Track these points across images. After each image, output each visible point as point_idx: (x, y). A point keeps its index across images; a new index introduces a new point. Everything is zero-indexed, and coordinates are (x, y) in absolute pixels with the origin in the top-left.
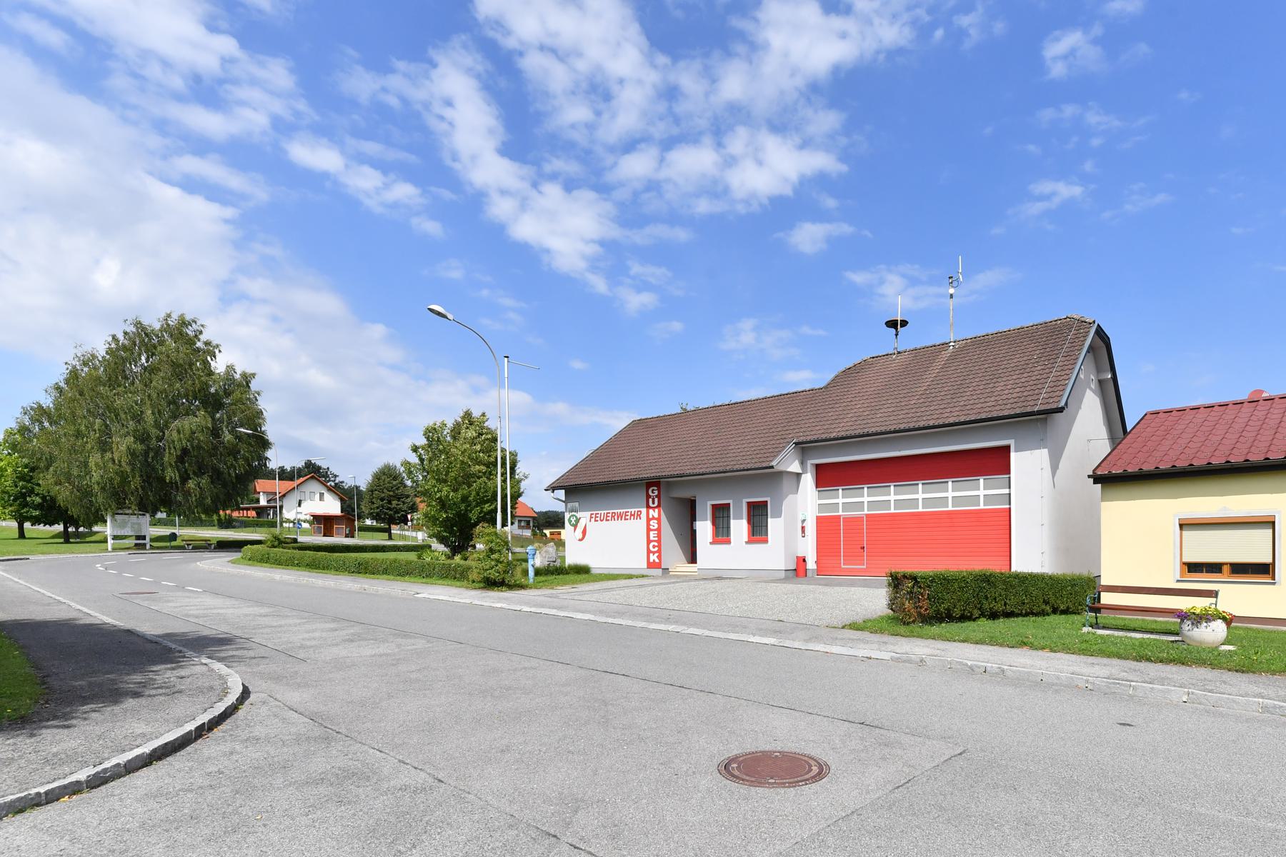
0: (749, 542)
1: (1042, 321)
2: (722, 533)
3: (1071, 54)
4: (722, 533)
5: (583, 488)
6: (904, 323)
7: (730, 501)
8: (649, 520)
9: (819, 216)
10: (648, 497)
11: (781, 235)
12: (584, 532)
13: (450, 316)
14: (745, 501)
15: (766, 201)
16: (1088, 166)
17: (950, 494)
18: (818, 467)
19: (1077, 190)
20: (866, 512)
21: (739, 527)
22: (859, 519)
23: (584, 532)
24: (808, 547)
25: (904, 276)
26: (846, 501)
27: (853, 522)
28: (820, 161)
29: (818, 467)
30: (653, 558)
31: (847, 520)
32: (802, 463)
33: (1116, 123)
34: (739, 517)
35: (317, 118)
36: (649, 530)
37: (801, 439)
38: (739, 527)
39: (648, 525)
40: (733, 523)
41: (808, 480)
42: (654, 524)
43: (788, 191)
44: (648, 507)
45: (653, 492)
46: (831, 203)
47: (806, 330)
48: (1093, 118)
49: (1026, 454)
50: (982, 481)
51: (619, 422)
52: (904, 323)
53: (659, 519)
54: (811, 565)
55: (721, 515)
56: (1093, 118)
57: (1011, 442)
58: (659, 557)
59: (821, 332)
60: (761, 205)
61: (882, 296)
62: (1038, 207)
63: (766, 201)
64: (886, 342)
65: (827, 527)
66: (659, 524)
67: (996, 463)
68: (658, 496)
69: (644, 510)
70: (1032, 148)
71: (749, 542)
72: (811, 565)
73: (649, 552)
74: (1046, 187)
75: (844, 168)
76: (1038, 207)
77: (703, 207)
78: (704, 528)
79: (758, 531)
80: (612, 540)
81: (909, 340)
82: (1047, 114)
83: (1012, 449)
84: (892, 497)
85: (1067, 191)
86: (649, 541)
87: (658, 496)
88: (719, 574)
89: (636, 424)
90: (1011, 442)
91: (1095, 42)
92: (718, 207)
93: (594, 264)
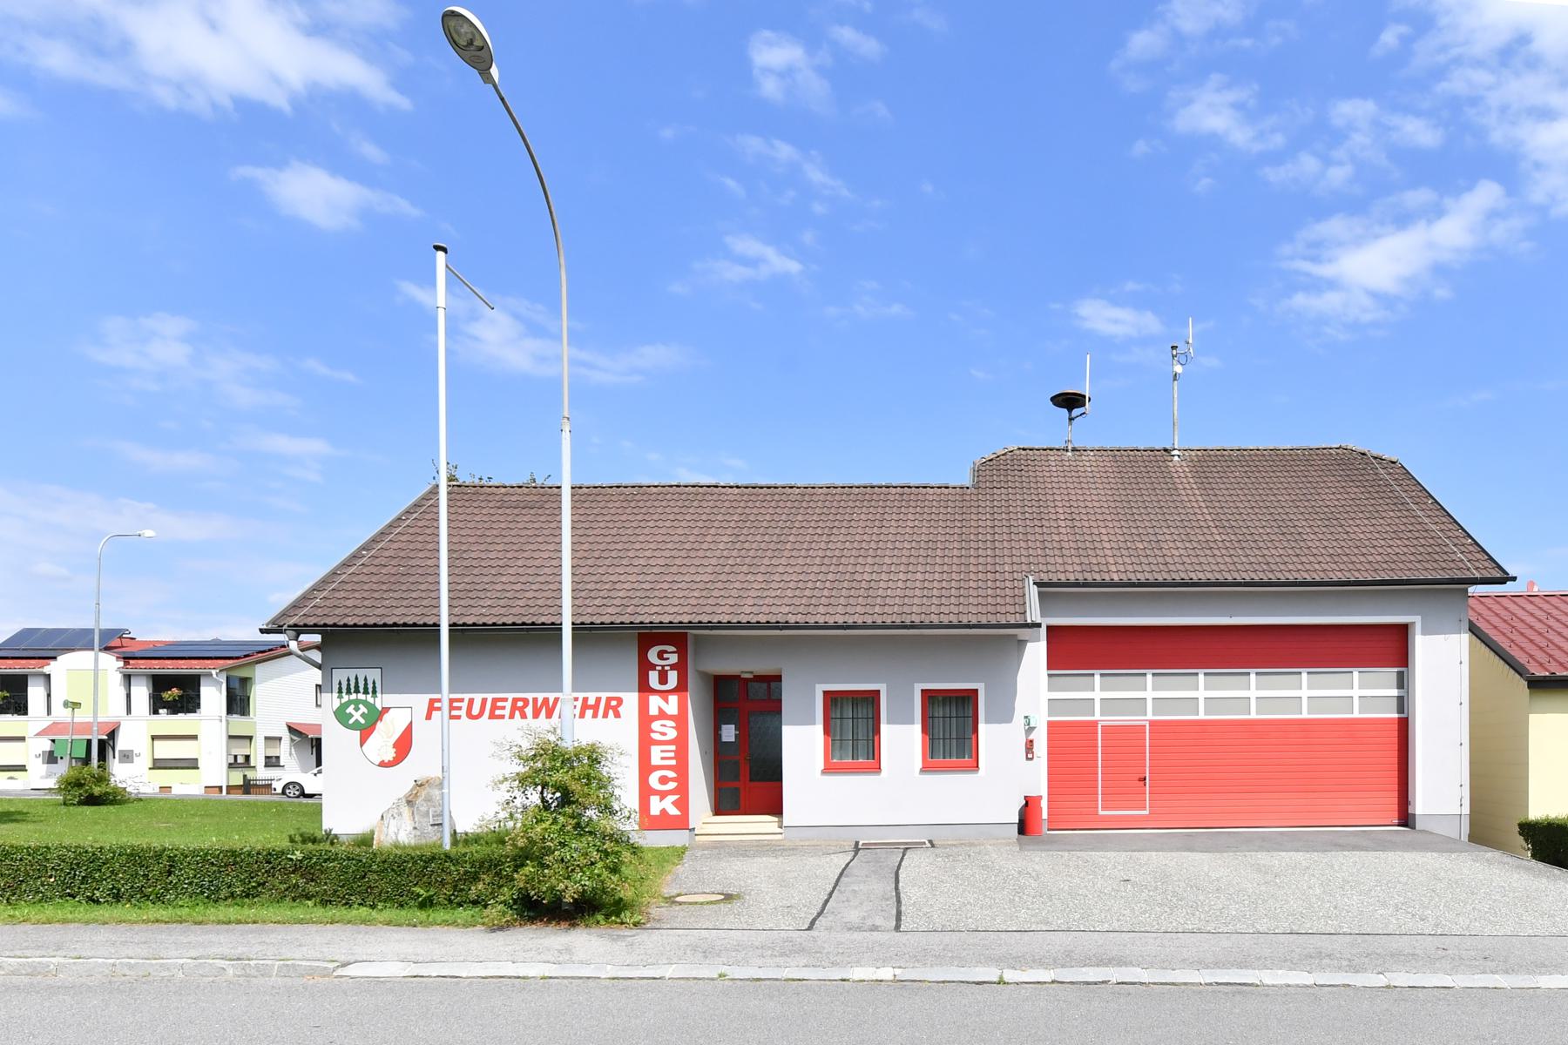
0: (926, 769)
1: (1304, 445)
3: (787, 73)
8: (645, 720)
9: (341, 163)
10: (645, 667)
11: (258, 173)
14: (918, 687)
15: (227, 103)
16: (808, 237)
17: (1201, 694)
19: (794, 267)
20: (1150, 716)
21: (902, 739)
24: (1036, 779)
25: (516, 316)
26: (1105, 697)
27: (1123, 737)
28: (345, 69)
33: (845, 193)
38: (902, 739)
40: (889, 733)
41: (1036, 652)
43: (279, 101)
44: (644, 688)
45: (663, 657)
46: (371, 152)
47: (313, 365)
48: (815, 175)
49: (1438, 640)
50: (1356, 674)
53: (680, 721)
56: (815, 175)
59: (349, 377)
60: (215, 106)
61: (476, 339)
62: (736, 273)
63: (227, 103)
65: (1069, 745)
67: (1392, 647)
69: (631, 699)
70: (731, 183)
71: (926, 769)
74: (747, 245)
75: (404, 103)
76: (736, 273)
77: (58, 59)
78: (802, 744)
81: (1087, 431)
82: (753, 144)
83: (1418, 628)
84: (1253, 693)
85: (780, 263)
87: (681, 667)
91: (820, 70)
92: (106, 75)
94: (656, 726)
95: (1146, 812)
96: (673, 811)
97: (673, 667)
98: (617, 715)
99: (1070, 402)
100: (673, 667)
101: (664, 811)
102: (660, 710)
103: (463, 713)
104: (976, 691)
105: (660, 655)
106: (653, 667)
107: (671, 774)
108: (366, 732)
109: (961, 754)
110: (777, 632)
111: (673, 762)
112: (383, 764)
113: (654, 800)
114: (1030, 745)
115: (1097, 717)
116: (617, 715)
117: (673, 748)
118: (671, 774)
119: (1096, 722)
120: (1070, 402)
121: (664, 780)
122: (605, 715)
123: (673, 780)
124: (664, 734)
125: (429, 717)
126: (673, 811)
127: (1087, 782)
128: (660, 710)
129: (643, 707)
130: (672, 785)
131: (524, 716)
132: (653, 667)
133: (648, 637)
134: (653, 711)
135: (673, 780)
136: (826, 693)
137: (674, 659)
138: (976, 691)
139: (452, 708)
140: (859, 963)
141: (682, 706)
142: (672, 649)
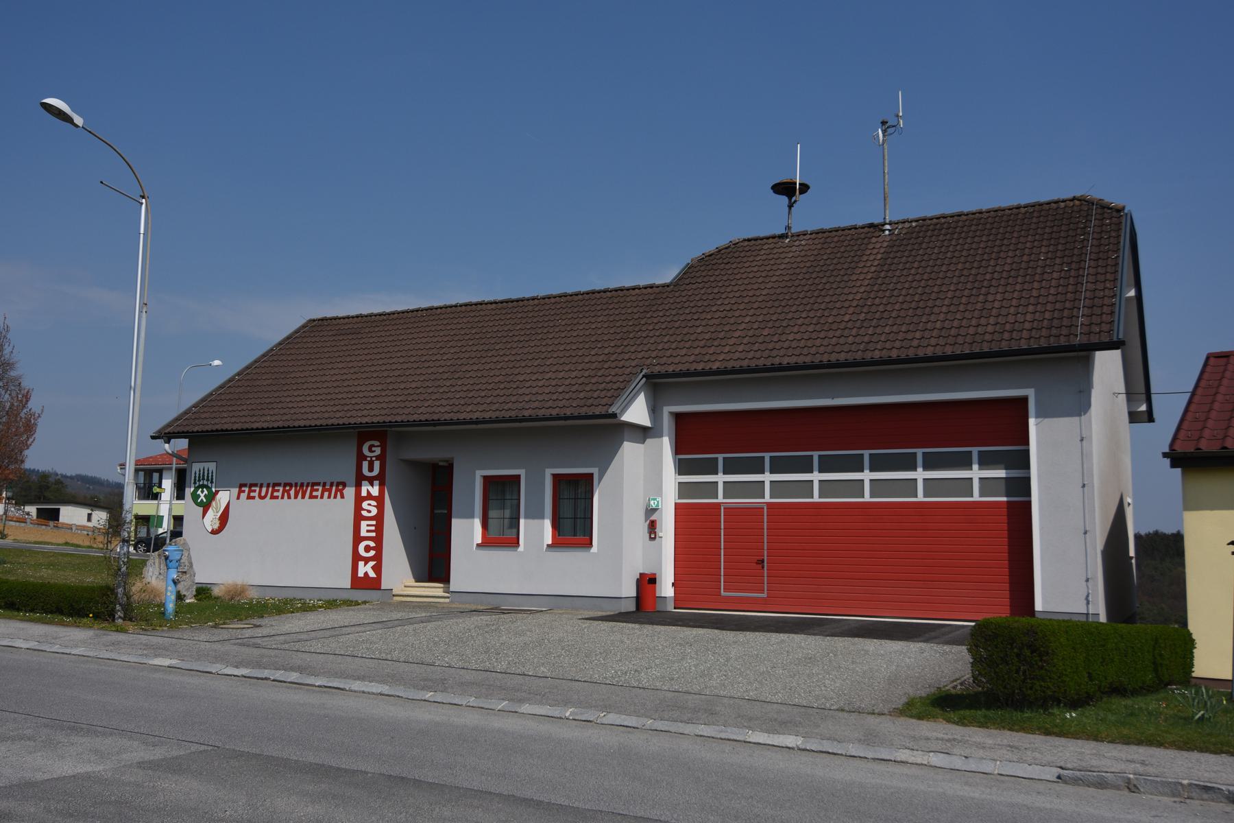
0: (556, 544)
2: (501, 537)
4: (501, 537)
5: (233, 436)
6: (805, 188)
7: (522, 472)
8: (359, 500)
10: (361, 457)
12: (224, 518)
13: (79, 120)
18: (679, 418)
20: (767, 499)
22: (755, 511)
23: (224, 518)
29: (679, 418)
30: (364, 569)
31: (731, 511)
32: (654, 410)
34: (538, 515)
35: (1103, 619)
36: (358, 518)
37: (657, 369)
38: (537, 531)
39: (358, 508)
42: (370, 508)
45: (372, 450)
51: (273, 321)
52: (805, 188)
54: (666, 589)
55: (501, 491)
57: (1030, 393)
58: (378, 569)
64: (770, 216)
66: (381, 507)
67: (1002, 431)
68: (381, 458)
71: (556, 544)
72: (666, 589)
73: (356, 558)
78: (467, 532)
79: (573, 527)
80: (283, 537)
81: (810, 215)
86: (357, 539)
87: (381, 458)
88: (495, 601)
89: (316, 327)
90: (1030, 393)
93: (1013, 613)
94: (365, 505)
95: (765, 595)
96: (372, 574)
97: (378, 458)
98: (342, 497)
99: (786, 189)
100: (378, 458)
101: (366, 574)
102: (368, 492)
103: (256, 494)
104: (518, 477)
105: (370, 451)
106: (365, 458)
107: (372, 544)
108: (206, 507)
109: (580, 537)
110: (474, 426)
111: (374, 534)
112: (214, 532)
113: (361, 564)
114: (652, 526)
115: (720, 499)
116: (342, 497)
117: (374, 523)
118: (372, 544)
119: (719, 505)
120: (786, 189)
121: (367, 549)
122: (296, 497)
123: (373, 548)
124: (369, 511)
125: (238, 498)
126: (372, 574)
127: (726, 571)
128: (368, 492)
129: (358, 492)
130: (372, 553)
131: (289, 497)
132: (365, 458)
133: (365, 433)
134: (364, 493)
135: (373, 548)
136: (555, 476)
137: (378, 451)
138: (518, 477)
139: (250, 491)
140: (156, 656)
141: (381, 492)
142: (377, 443)
